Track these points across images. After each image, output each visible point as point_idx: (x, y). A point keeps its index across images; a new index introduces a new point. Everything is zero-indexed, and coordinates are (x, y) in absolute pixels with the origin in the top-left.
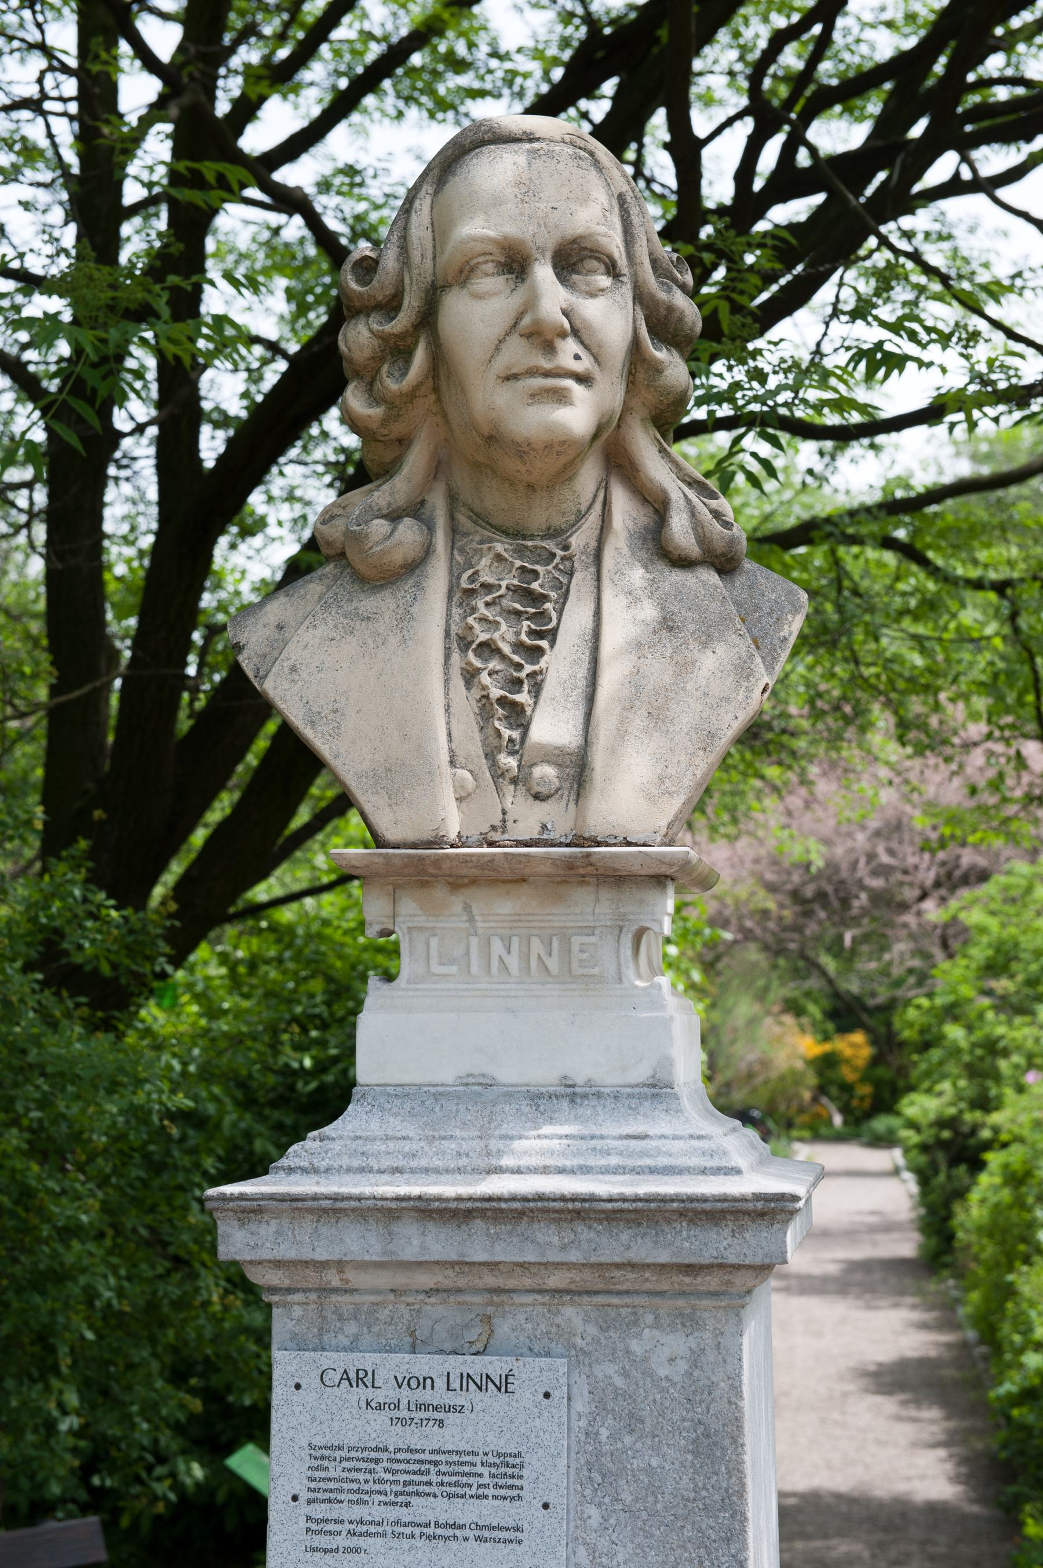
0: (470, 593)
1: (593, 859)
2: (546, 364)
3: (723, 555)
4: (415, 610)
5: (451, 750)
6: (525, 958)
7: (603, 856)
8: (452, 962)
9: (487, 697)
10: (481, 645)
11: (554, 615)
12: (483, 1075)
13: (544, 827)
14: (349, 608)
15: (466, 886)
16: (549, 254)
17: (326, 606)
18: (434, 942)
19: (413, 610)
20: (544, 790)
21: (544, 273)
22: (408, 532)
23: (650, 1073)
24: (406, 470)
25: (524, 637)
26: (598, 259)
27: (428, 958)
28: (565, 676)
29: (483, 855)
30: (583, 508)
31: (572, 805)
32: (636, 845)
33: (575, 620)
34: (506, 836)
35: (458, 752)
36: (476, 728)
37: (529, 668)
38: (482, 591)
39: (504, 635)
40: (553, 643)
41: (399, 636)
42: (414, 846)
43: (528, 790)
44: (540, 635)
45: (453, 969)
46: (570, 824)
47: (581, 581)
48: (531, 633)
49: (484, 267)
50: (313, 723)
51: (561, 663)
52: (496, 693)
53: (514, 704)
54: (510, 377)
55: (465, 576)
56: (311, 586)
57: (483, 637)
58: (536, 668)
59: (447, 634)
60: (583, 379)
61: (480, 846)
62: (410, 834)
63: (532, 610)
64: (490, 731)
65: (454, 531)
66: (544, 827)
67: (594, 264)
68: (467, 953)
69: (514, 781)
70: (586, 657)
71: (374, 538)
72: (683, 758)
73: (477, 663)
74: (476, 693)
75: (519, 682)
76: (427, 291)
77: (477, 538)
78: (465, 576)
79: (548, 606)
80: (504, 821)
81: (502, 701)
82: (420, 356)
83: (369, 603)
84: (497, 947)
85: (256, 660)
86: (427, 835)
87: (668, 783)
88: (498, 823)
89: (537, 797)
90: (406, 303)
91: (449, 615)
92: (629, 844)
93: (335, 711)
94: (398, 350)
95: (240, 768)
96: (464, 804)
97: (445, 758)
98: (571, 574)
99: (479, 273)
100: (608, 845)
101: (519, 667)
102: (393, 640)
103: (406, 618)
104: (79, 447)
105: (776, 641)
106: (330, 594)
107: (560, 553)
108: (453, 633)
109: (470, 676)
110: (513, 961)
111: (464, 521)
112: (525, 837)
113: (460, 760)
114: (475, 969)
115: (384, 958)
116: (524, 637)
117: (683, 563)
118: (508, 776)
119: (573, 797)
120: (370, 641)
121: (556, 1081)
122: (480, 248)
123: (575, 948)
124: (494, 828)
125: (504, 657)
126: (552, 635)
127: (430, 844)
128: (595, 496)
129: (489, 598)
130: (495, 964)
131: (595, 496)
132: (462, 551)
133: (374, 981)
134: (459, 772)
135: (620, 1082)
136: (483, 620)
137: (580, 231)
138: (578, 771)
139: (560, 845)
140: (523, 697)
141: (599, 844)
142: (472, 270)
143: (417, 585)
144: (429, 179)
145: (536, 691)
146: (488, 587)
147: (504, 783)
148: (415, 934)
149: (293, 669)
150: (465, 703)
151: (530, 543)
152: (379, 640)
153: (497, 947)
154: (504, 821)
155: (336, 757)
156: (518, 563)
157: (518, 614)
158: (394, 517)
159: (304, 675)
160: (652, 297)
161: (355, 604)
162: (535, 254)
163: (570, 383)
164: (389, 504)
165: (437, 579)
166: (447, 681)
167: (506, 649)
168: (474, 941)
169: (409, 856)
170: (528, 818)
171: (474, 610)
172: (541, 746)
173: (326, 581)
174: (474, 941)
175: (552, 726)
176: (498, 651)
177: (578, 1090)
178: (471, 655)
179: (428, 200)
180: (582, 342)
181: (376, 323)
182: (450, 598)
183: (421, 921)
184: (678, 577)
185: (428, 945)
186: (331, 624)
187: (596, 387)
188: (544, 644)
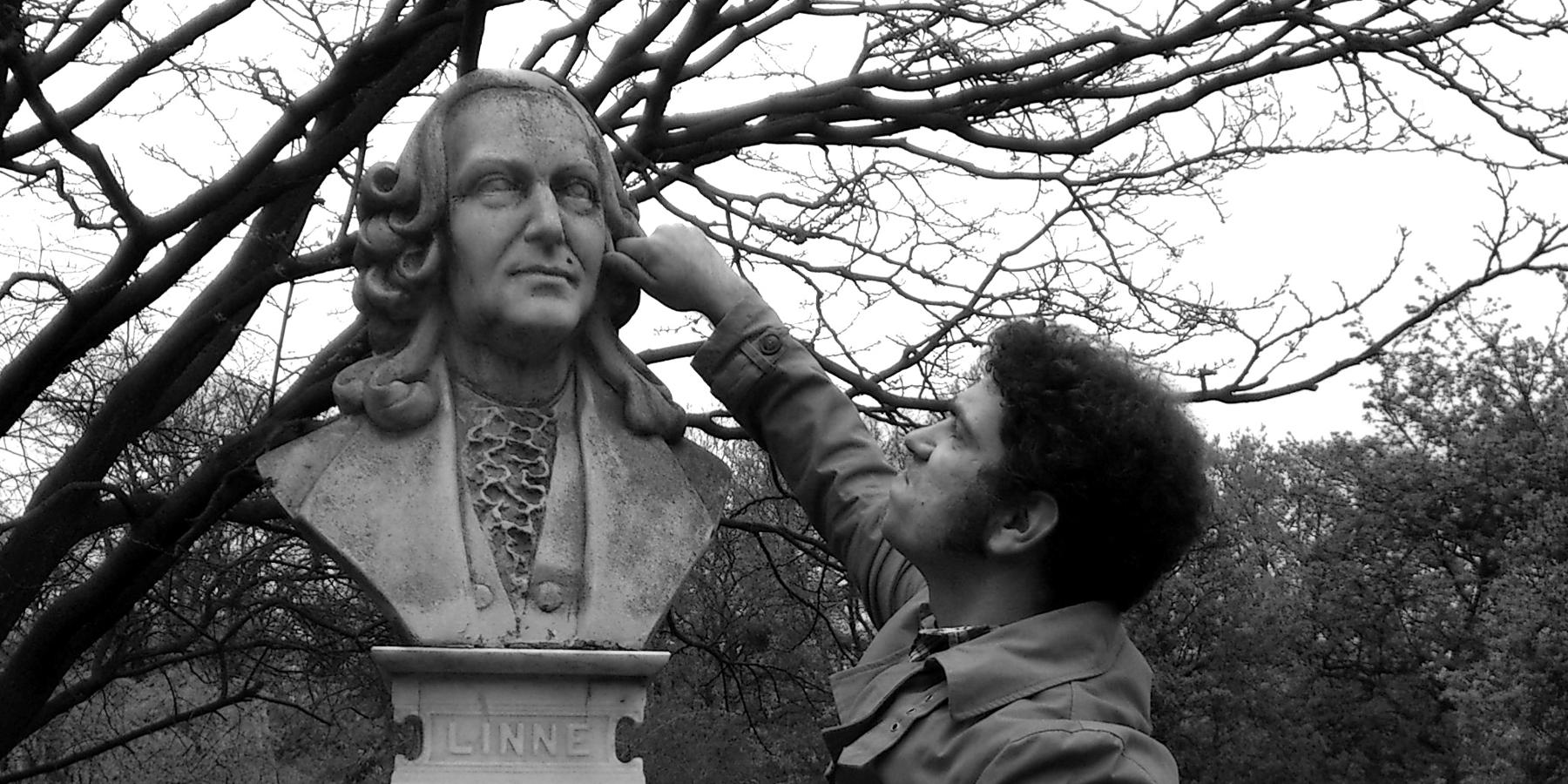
2: (548, 265)
4: (432, 456)
6: (529, 742)
8: (469, 743)
9: (499, 528)
10: (491, 486)
18: (452, 725)
19: (432, 456)
21: (544, 193)
24: (414, 345)
25: (525, 482)
31: (572, 617)
33: (562, 474)
37: (531, 507)
40: (548, 486)
45: (469, 749)
51: (555, 498)
52: (507, 525)
53: (523, 533)
54: (514, 273)
55: (471, 432)
57: (492, 480)
59: (459, 476)
60: (572, 279)
64: (503, 554)
65: (455, 396)
67: (581, 189)
68: (481, 737)
69: (525, 596)
73: (488, 501)
74: (489, 524)
75: (525, 517)
78: (471, 432)
79: (541, 458)
81: (512, 531)
82: (433, 252)
83: (389, 449)
84: (507, 732)
89: (545, 609)
90: (423, 208)
91: (458, 464)
92: (620, 649)
95: (13, 635)
97: (466, 576)
101: (523, 505)
102: (416, 479)
103: (425, 462)
104: (241, 231)
107: (546, 419)
109: (483, 510)
111: (464, 390)
112: (536, 641)
113: (478, 578)
114: (487, 748)
115: (409, 739)
116: (525, 482)
117: (644, 433)
123: (571, 732)
124: (510, 634)
125: (510, 497)
126: (547, 481)
129: (493, 450)
132: (465, 413)
136: (490, 467)
137: (571, 162)
138: (577, 591)
140: (529, 529)
145: (538, 524)
146: (490, 442)
150: (480, 535)
156: (513, 424)
157: (517, 463)
163: (562, 280)
165: (446, 431)
166: (463, 514)
167: (511, 491)
170: (538, 626)
171: (480, 459)
172: (547, 569)
175: (551, 553)
176: (505, 492)
178: (483, 496)
182: (458, 449)
188: (542, 488)
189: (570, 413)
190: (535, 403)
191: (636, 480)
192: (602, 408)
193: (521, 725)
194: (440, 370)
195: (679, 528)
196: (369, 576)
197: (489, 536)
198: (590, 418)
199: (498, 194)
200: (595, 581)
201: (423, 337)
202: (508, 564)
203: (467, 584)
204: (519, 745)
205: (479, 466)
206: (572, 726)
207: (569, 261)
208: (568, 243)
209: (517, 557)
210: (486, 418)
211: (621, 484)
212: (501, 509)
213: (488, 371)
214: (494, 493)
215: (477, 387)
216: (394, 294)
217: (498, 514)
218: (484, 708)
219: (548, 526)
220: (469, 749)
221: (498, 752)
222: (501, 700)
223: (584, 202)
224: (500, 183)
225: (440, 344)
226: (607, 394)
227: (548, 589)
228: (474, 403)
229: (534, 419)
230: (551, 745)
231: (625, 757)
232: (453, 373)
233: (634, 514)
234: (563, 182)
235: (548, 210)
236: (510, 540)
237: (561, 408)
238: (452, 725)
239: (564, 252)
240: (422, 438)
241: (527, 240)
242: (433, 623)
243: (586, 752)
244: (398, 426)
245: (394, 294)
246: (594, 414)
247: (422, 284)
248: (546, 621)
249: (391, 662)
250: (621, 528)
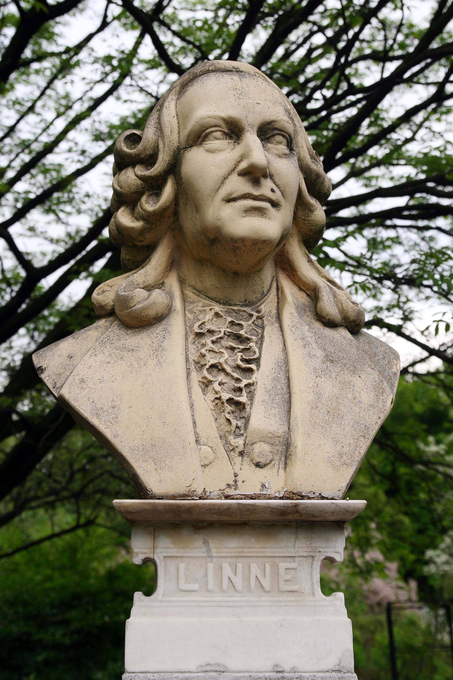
0: (199, 335)
1: (300, 508)
2: (256, 193)
3: (354, 321)
4: (165, 344)
5: (196, 433)
6: (247, 579)
7: (307, 507)
9: (219, 399)
11: (257, 350)
12: (218, 665)
13: (263, 486)
14: (120, 344)
15: (205, 528)
16: (255, 129)
17: (103, 343)
18: (182, 566)
20: (263, 460)
21: (251, 139)
22: (158, 296)
23: (336, 661)
25: (240, 363)
26: (283, 136)
27: (178, 578)
28: (270, 387)
29: (222, 505)
30: (265, 291)
31: (282, 471)
32: (327, 499)
33: (269, 354)
34: (237, 492)
35: (201, 434)
36: (213, 419)
37: (245, 382)
38: (208, 334)
39: (227, 359)
40: (258, 366)
41: (156, 360)
42: (174, 497)
43: (252, 460)
44: (248, 361)
45: (196, 587)
46: (282, 484)
47: (271, 332)
48: (243, 360)
49: (215, 134)
50: (98, 415)
51: (263, 376)
52: (226, 396)
54: (230, 200)
56: (90, 332)
57: (213, 362)
58: (250, 381)
59: (187, 360)
60: (275, 204)
61: (220, 498)
62: (171, 489)
63: (242, 347)
64: (223, 421)
65: (184, 299)
66: (263, 486)
68: (206, 576)
69: (241, 454)
70: (282, 376)
71: (137, 299)
72: (352, 441)
73: (210, 377)
74: (211, 396)
76: (174, 152)
77: (201, 304)
79: (252, 344)
80: (236, 481)
81: (230, 401)
82: (168, 191)
84: (227, 571)
85: (54, 377)
86: (182, 490)
87: (345, 458)
88: (232, 483)
89: (258, 465)
92: (323, 498)
93: (113, 407)
94: (154, 186)
96: (207, 469)
97: (192, 439)
98: (263, 328)
99: (211, 137)
100: (309, 498)
101: (238, 380)
102: (152, 363)
103: (159, 349)
105: (391, 374)
106: (105, 336)
107: (255, 314)
108: (191, 360)
109: (206, 384)
110: (238, 581)
111: (189, 293)
113: (203, 439)
115: (145, 580)
116: (240, 363)
117: (330, 324)
118: (237, 450)
119: (282, 466)
120: (135, 363)
121: (270, 669)
122: (213, 121)
123: (282, 571)
124: (229, 486)
125: (227, 374)
126: (257, 361)
127: (184, 496)
128: (271, 285)
129: (214, 338)
130: (253, 581)
131: (271, 285)
132: (191, 312)
133: (138, 596)
134: (203, 447)
135: (316, 668)
138: (286, 450)
139: (275, 498)
140: (243, 399)
141: (303, 497)
142: (207, 136)
143: (165, 330)
144: (173, 92)
146: (211, 332)
147: (235, 455)
148: (168, 560)
149: (82, 381)
150: (204, 403)
151: (236, 308)
152: (142, 363)
153: (227, 571)
154: (236, 481)
155: (115, 437)
156: (229, 319)
157: (233, 349)
158: (149, 288)
159: (90, 384)
160: (308, 167)
161: (122, 342)
162: (247, 127)
163: (267, 205)
164: (144, 282)
165: (176, 325)
166: (189, 389)
167: (228, 369)
168: (211, 566)
169: (170, 505)
173: (100, 330)
174: (211, 566)
175: (263, 417)
176: (223, 370)
177: (286, 675)
178: (205, 373)
179: (173, 103)
180: (275, 183)
181: (140, 170)
182: (186, 339)
183: (173, 551)
184: (328, 332)
185: (178, 569)
186: (107, 354)
187: (282, 210)
188: (253, 366)
189: (274, 311)
190: (248, 303)
191: (329, 359)
192: (300, 309)
193: (240, 565)
194: (173, 282)
195: (367, 397)
196: (113, 440)
197: (212, 405)
198: (290, 314)
199: (217, 142)
200: (299, 441)
201: (159, 258)
202: (227, 428)
203: (193, 443)
204: (238, 581)
205: (203, 351)
206: (283, 565)
207: (273, 191)
208: (271, 177)
209: (234, 422)
210: (210, 315)
211: (317, 363)
212: (220, 384)
213: (209, 281)
214: (215, 370)
215: (201, 292)
216: (138, 224)
217: (218, 388)
218: (209, 551)
219: (258, 397)
220: (196, 587)
221: (222, 590)
222: (227, 548)
223: (283, 148)
224: (218, 134)
225: (173, 264)
226: (302, 298)
227: (261, 450)
228: (200, 303)
229: (246, 315)
230: (266, 583)
231: (327, 588)
232: (182, 282)
233: (328, 387)
234: (267, 132)
235: (255, 150)
236: (229, 408)
237: (268, 306)
238: (182, 566)
239: (267, 184)
240: (158, 329)
241: (239, 175)
242: (164, 477)
243: (295, 588)
244: (138, 322)
245: (138, 224)
246: (293, 311)
247: (159, 215)
248: (261, 474)
249: (126, 513)
250: (319, 396)
